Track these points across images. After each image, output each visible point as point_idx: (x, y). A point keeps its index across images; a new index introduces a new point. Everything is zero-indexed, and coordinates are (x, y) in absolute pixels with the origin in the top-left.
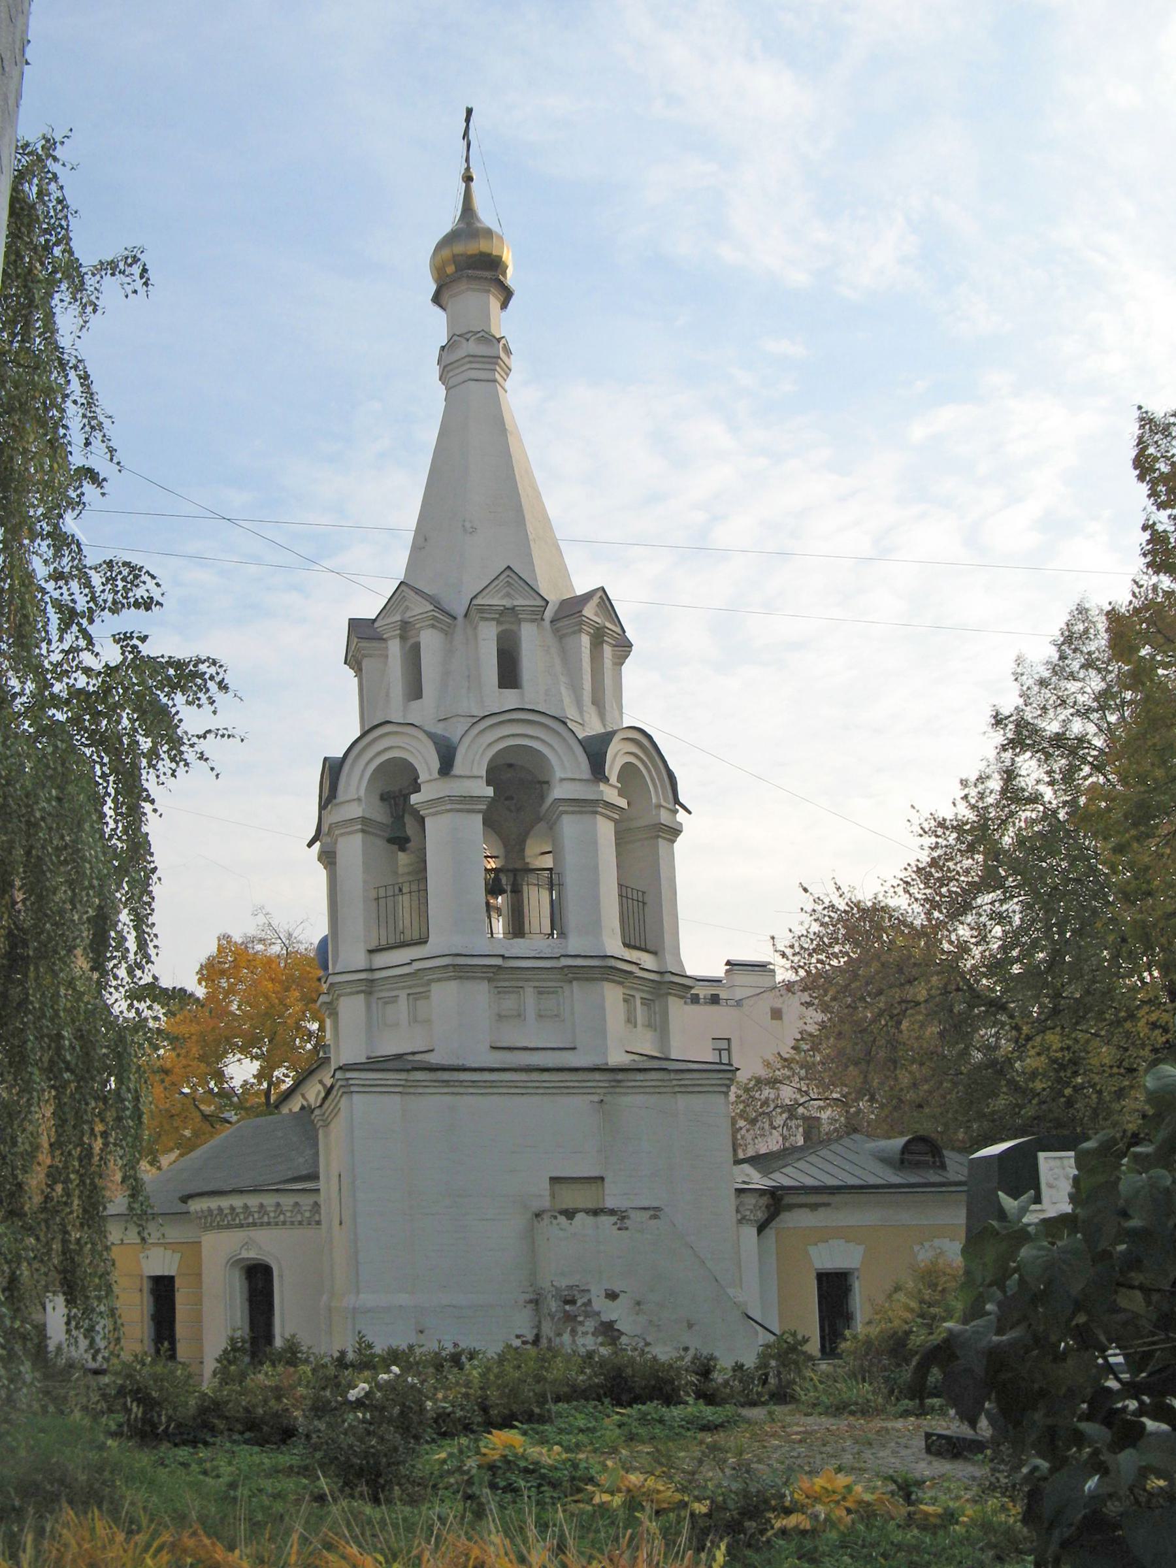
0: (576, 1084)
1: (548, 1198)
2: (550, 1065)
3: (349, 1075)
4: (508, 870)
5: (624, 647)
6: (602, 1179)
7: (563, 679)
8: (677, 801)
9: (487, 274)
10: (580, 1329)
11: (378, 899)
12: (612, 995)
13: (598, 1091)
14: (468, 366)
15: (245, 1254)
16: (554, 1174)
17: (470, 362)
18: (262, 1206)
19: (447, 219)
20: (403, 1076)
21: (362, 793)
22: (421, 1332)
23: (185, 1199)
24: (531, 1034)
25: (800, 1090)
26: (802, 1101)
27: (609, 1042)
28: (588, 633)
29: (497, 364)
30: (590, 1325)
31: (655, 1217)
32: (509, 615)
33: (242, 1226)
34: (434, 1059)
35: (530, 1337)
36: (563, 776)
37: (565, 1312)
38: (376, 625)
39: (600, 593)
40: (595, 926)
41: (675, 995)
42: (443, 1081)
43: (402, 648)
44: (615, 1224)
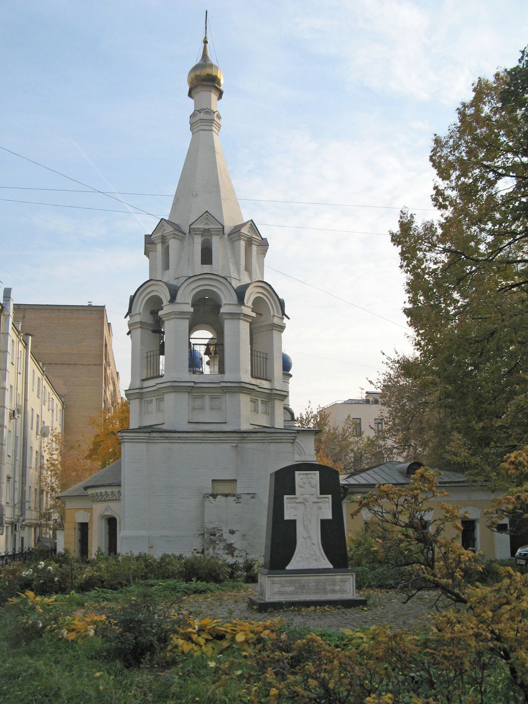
0: (225, 439)
1: (211, 489)
2: (215, 430)
3: (123, 434)
4: (213, 345)
5: (264, 244)
6: (236, 480)
7: (231, 260)
8: (283, 314)
9: (210, 84)
10: (217, 547)
11: (147, 357)
12: (245, 400)
13: (235, 441)
14: (200, 124)
15: (106, 513)
16: (213, 479)
17: (201, 122)
18: (112, 492)
19: (196, 59)
20: (147, 435)
21: (141, 311)
22: (152, 547)
23: (86, 488)
24: (208, 416)
25: (395, 441)
26: (396, 446)
27: (242, 420)
28: (244, 240)
29: (213, 123)
30: (222, 545)
31: (253, 497)
32: (206, 232)
33: (105, 501)
34: (164, 427)
35: (200, 550)
36: (226, 303)
37: (211, 539)
38: (152, 237)
39: (251, 222)
40: (237, 368)
41: (279, 399)
42: (165, 437)
43: (162, 247)
44: (235, 500)
